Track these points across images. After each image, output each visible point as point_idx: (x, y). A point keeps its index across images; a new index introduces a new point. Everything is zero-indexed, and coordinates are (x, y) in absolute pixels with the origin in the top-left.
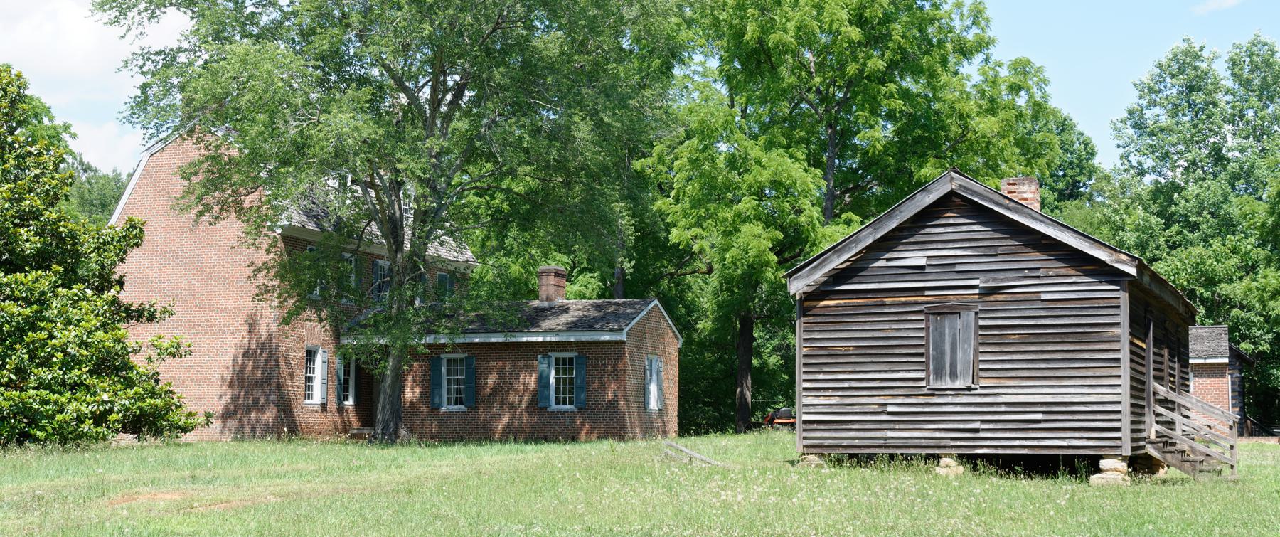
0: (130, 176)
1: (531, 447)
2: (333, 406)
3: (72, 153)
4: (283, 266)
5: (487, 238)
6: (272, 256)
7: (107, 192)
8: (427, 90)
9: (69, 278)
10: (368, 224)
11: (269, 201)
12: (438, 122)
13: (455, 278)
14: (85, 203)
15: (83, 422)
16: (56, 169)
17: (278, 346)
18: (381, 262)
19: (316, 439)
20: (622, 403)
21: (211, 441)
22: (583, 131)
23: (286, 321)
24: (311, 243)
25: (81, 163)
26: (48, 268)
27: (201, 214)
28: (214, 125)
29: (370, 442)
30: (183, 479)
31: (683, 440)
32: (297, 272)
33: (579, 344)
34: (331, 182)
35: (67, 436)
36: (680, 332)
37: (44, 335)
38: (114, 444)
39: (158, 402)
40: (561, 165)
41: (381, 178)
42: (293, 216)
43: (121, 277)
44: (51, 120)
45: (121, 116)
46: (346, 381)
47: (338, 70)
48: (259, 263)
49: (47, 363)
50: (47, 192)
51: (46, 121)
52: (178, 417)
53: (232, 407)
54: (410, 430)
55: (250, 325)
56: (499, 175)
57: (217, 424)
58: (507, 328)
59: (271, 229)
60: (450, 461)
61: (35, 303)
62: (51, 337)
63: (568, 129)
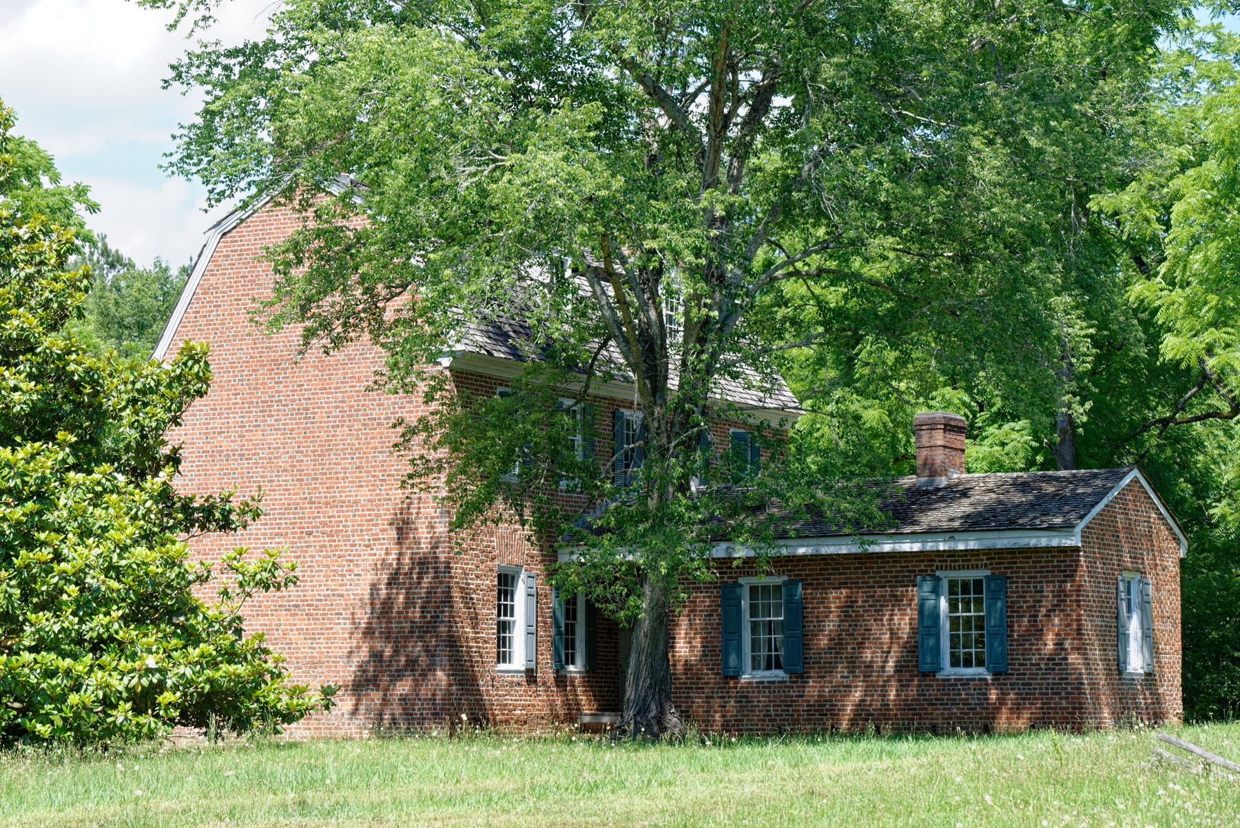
0: (187, 272)
1: (906, 747)
3: (87, 239)
5: (821, 361)
6: (434, 406)
7: (147, 302)
8: (703, 100)
9: (87, 454)
10: (604, 345)
12: (725, 156)
13: (760, 440)
14: (112, 325)
15: (115, 707)
16: (61, 265)
17: (448, 567)
18: (627, 412)
20: (1073, 658)
21: (338, 740)
22: (988, 165)
24: (502, 382)
25: (105, 252)
26: (51, 437)
27: (309, 334)
29: (614, 738)
30: (284, 806)
31: (1191, 730)
33: (993, 555)
35: (89, 734)
36: (1184, 529)
37: (46, 554)
38: (167, 745)
39: (241, 669)
40: (948, 230)
41: (624, 262)
42: (469, 339)
43: (175, 451)
44: (55, 179)
45: (165, 162)
46: (570, 629)
47: (541, 70)
48: (412, 420)
49: (51, 603)
50: (46, 305)
51: (45, 180)
52: (276, 695)
54: (686, 716)
55: (399, 529)
57: (345, 704)
58: (861, 527)
59: (433, 359)
60: (758, 774)
61: (28, 499)
62: (58, 557)
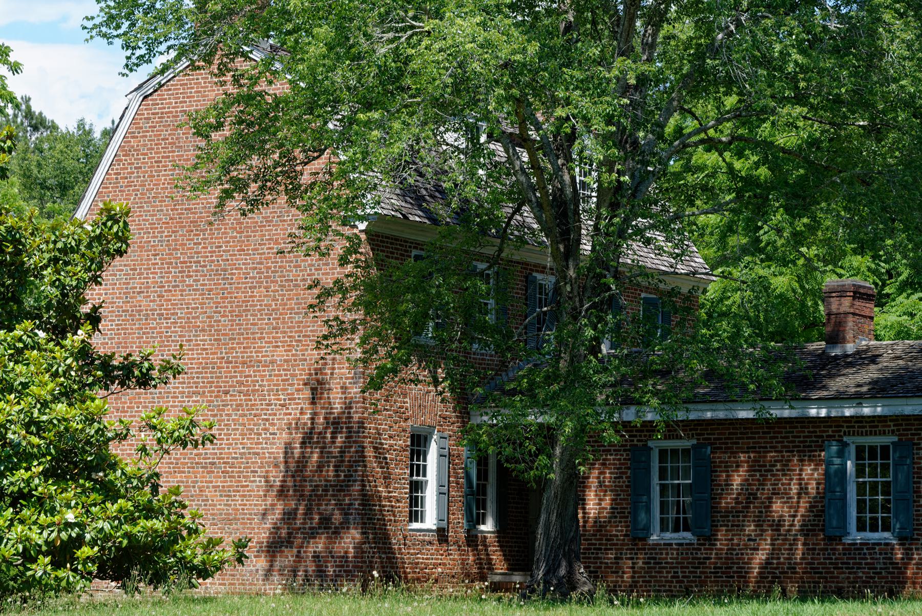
0: (109, 134)
2: (458, 532)
4: (370, 287)
5: (730, 229)
6: (349, 268)
7: (69, 164)
10: (517, 210)
11: (343, 174)
13: (670, 305)
15: (34, 560)
17: (361, 424)
19: (429, 591)
23: (375, 384)
24: (417, 245)
25: (29, 114)
27: (227, 195)
28: (246, 41)
32: (395, 299)
34: (450, 137)
38: (84, 598)
41: (538, 127)
42: (385, 200)
43: (95, 309)
45: (89, 24)
46: (482, 490)
48: (328, 281)
52: (193, 551)
53: (284, 532)
54: (594, 575)
55: (313, 390)
56: (748, 115)
57: (257, 563)
63: (873, 35)
